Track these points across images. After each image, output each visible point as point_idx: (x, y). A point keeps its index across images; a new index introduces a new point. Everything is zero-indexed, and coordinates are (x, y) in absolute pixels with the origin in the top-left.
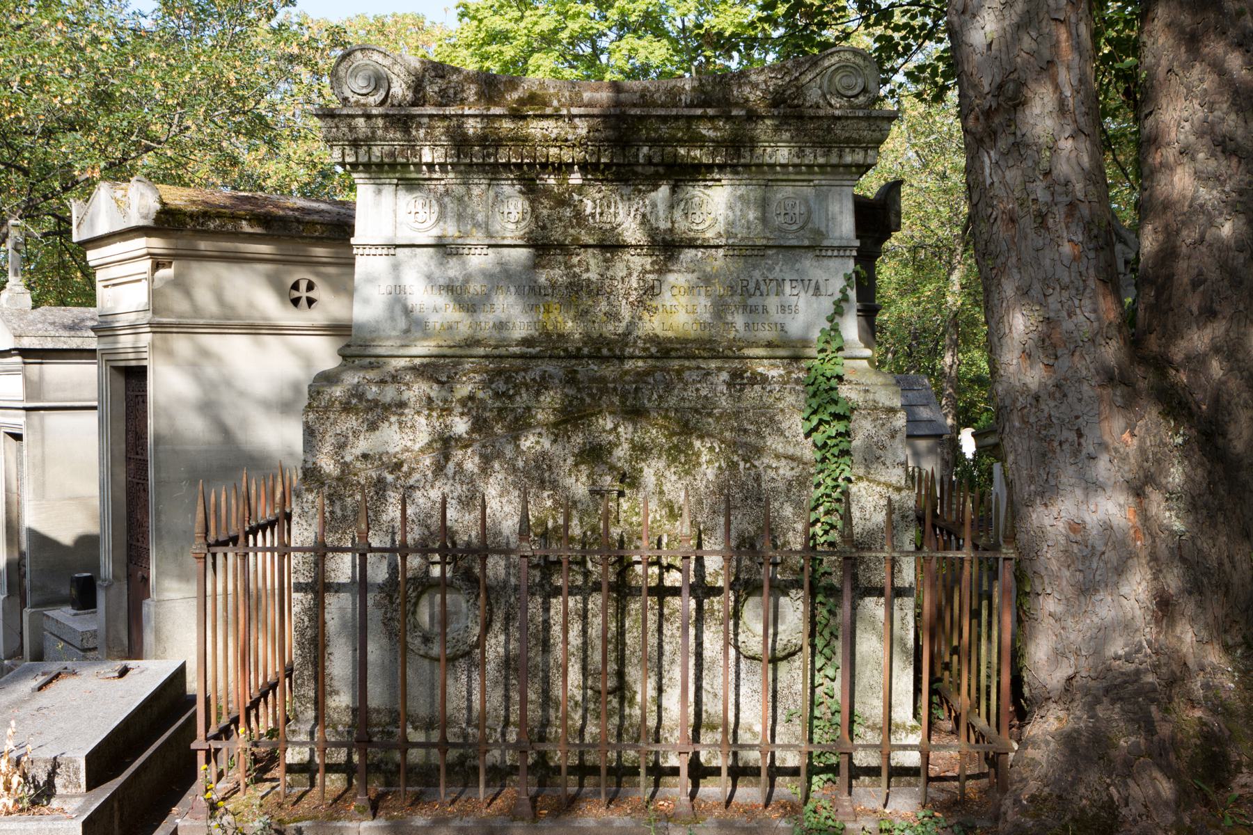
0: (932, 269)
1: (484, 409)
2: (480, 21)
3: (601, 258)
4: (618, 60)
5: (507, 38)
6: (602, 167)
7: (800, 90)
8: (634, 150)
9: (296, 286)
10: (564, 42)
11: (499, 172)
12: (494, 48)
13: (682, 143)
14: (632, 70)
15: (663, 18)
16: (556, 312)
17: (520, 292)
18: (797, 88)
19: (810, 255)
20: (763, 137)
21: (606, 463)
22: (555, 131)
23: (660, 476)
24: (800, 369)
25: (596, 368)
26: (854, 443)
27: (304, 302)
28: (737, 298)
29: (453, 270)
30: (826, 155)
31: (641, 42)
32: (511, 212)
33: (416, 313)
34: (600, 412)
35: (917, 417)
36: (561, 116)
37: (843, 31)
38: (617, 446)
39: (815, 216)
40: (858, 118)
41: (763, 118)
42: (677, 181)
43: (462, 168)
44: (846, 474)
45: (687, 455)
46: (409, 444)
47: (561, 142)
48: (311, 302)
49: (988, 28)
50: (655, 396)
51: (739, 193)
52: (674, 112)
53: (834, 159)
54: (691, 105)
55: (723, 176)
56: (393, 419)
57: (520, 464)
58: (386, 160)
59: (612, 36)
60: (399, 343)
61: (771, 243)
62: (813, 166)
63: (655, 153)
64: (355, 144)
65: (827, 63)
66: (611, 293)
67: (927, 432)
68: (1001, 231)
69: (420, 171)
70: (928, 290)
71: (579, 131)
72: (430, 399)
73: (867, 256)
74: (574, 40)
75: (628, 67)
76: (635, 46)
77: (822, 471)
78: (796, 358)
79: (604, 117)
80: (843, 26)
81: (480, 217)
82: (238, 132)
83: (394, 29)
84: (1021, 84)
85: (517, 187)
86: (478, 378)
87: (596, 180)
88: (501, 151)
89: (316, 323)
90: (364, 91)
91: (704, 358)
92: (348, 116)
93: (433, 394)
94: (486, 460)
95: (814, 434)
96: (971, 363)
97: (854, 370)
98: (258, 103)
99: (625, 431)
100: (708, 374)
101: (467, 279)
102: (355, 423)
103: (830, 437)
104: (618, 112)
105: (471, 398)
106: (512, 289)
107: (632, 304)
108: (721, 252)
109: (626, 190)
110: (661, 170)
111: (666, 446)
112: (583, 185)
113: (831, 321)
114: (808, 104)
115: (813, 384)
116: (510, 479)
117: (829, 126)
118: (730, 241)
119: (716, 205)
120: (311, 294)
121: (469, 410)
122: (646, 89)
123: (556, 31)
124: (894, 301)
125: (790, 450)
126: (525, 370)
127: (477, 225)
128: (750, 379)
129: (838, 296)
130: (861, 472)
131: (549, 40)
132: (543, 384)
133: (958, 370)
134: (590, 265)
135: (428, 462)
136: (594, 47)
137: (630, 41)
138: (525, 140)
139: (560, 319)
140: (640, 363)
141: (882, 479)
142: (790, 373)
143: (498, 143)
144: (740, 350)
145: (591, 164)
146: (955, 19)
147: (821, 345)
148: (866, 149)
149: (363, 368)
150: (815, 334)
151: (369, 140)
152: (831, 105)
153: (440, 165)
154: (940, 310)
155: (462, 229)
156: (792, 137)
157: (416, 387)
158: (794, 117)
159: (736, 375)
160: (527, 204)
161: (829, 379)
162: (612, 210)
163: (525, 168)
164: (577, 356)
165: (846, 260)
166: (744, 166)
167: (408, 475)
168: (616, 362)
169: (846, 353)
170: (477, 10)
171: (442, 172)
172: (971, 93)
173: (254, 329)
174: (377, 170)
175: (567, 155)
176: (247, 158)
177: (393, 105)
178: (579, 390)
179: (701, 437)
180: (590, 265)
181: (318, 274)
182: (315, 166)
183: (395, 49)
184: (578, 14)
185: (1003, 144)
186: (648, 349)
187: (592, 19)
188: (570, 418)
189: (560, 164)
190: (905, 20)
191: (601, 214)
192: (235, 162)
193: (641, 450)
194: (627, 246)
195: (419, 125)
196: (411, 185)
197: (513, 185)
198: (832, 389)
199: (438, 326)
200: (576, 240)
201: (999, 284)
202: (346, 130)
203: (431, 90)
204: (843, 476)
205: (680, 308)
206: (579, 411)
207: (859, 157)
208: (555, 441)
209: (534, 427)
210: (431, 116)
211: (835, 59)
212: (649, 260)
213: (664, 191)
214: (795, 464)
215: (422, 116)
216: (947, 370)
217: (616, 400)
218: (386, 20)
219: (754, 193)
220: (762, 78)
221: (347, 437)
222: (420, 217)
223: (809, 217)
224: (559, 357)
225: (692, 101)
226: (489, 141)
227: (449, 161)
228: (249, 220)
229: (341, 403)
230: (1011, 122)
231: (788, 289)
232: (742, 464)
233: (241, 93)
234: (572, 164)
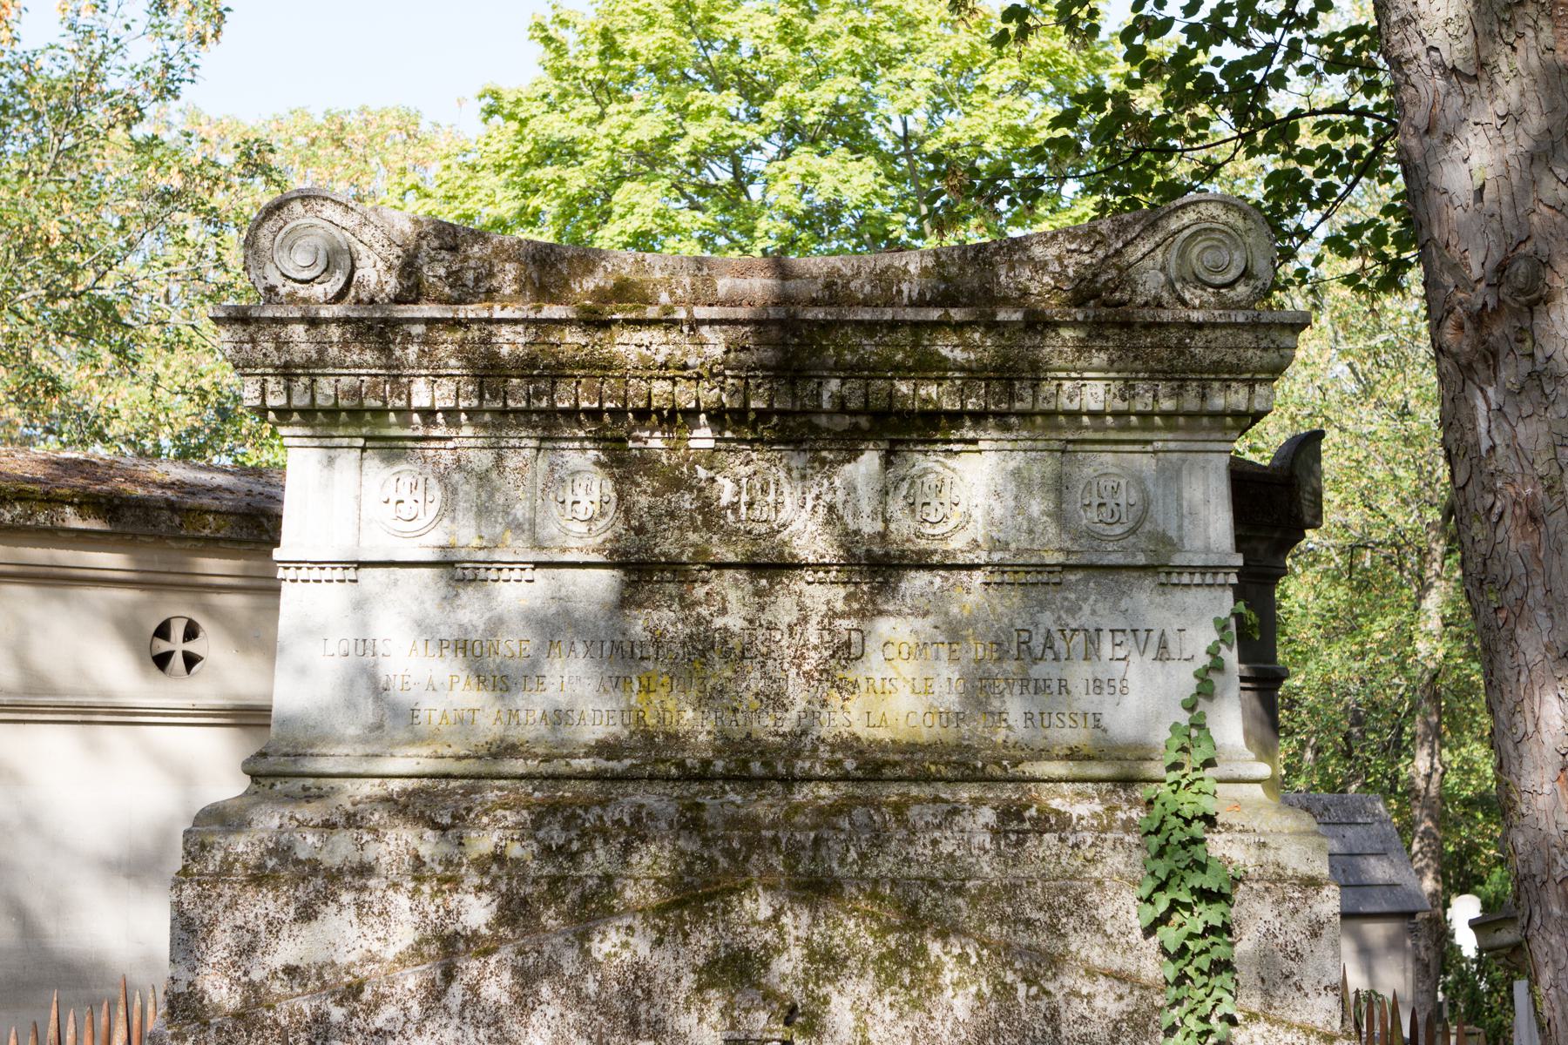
0: (1386, 587)
1: (523, 879)
2: (524, 122)
3: (749, 587)
4: (783, 195)
5: (573, 154)
6: (752, 416)
7: (1125, 277)
8: (812, 385)
9: (163, 631)
10: (682, 161)
11: (558, 427)
12: (547, 173)
13: (902, 371)
14: (808, 214)
15: (868, 116)
16: (663, 691)
17: (593, 645)
18: (1120, 270)
19: (1148, 582)
20: (1056, 362)
21: (758, 986)
22: (664, 350)
23: (863, 1012)
24: (1133, 803)
25: (738, 799)
26: (1239, 948)
27: (177, 662)
28: (1011, 666)
29: (470, 611)
30: (1177, 394)
31: (826, 162)
32: (578, 501)
33: (396, 693)
34: (747, 885)
35: (1365, 878)
36: (675, 322)
37: (1206, 161)
38: (779, 952)
39: (1157, 510)
40: (1236, 325)
41: (1056, 326)
42: (893, 442)
43: (487, 417)
44: (1227, 1007)
45: (914, 971)
46: (376, 947)
47: (675, 370)
48: (191, 660)
49: (1475, 161)
50: (853, 855)
51: (1012, 465)
52: (888, 315)
53: (1191, 402)
54: (920, 303)
55: (982, 435)
56: (346, 897)
57: (591, 987)
58: (344, 403)
59: (771, 150)
60: (360, 749)
61: (1073, 560)
62: (1152, 414)
63: (852, 390)
64: (287, 372)
65: (1174, 224)
66: (767, 656)
67: (1385, 908)
68: (1513, 539)
69: (407, 424)
70: (1380, 629)
71: (708, 350)
72: (418, 862)
73: (1257, 582)
74: (697, 160)
75: (799, 207)
76: (814, 169)
77: (1178, 1002)
78: (1126, 781)
79: (759, 324)
80: (1205, 153)
81: (521, 511)
82: (61, 332)
83: (361, 136)
84: (1543, 264)
85: (592, 454)
86: (511, 818)
87: (741, 441)
88: (561, 386)
89: (201, 703)
90: (306, 275)
91: (948, 781)
92: (275, 320)
93: (425, 851)
94: (527, 978)
95: (1162, 929)
96: (1468, 768)
97: (1238, 805)
98: (101, 276)
99: (797, 923)
100: (955, 811)
101: (496, 625)
102: (271, 906)
103: (1192, 936)
104: (782, 315)
105: (498, 857)
106: (580, 648)
107: (808, 676)
108: (979, 577)
109: (798, 461)
110: (864, 422)
111: (875, 953)
112: (715, 450)
113: (1191, 709)
114: (1140, 300)
115: (1158, 831)
116: (571, 1016)
117: (1180, 340)
118: (996, 557)
119: (973, 489)
120: (193, 647)
121: (494, 881)
122: (834, 272)
123: (666, 141)
124: (1315, 650)
125: (1116, 962)
126: (602, 804)
127: (516, 526)
128: (1035, 821)
129: (1206, 660)
130: (1255, 1004)
131: (651, 157)
132: (637, 831)
133: (1442, 783)
134: (729, 604)
135: (411, 983)
136: (737, 170)
137: (804, 158)
138: (607, 366)
139: (670, 705)
140: (824, 790)
141: (1296, 1019)
142: (1112, 809)
143: (557, 372)
144: (1015, 765)
145: (731, 411)
146: (1413, 142)
147: (1173, 756)
148: (1251, 384)
149: (290, 798)
150: (1161, 735)
151: (314, 366)
152: (1184, 303)
153: (447, 412)
154: (1403, 668)
155: (486, 532)
156: (1111, 362)
157: (391, 835)
158: (1114, 324)
159: (1010, 814)
160: (609, 485)
161: (1188, 823)
162: (771, 498)
163: (607, 418)
164: (703, 775)
165: (1218, 592)
166: (1021, 414)
167: (373, 1007)
168: (778, 787)
169: (1221, 771)
170: (518, 102)
171: (448, 424)
172: (1448, 280)
173: (88, 713)
174: (323, 420)
175: (686, 395)
176: (74, 375)
177: (359, 302)
178: (706, 843)
179: (942, 935)
180: (729, 604)
181: (209, 611)
182: (204, 395)
183: (363, 173)
184: (708, 111)
185: (1510, 373)
186: (839, 763)
187: (733, 118)
188: (692, 897)
189: (673, 412)
190: (1324, 139)
191: (750, 505)
192: (54, 387)
193: (826, 962)
194: (800, 566)
195: (408, 339)
196: (391, 449)
197: (584, 450)
198: (1195, 841)
199: (436, 718)
200: (701, 552)
201: (1512, 638)
202: (270, 346)
203: (434, 273)
204: (1219, 1011)
205: (899, 684)
206: (707, 883)
207: (1237, 398)
208: (659, 943)
209: (620, 915)
210: (430, 322)
211: (1189, 217)
212: (841, 591)
213: (869, 461)
214: (1125, 989)
215: (414, 321)
216: (1421, 784)
217: (777, 861)
218: (347, 119)
219: (1044, 467)
220: (1053, 251)
221: (256, 934)
222: (405, 511)
223: (1145, 511)
224: (668, 778)
225: (921, 294)
227: (463, 404)
228: (80, 506)
229: (245, 866)
230: (1524, 334)
231: (1106, 648)
232: (1022, 989)
233: (71, 258)
234: (695, 412)
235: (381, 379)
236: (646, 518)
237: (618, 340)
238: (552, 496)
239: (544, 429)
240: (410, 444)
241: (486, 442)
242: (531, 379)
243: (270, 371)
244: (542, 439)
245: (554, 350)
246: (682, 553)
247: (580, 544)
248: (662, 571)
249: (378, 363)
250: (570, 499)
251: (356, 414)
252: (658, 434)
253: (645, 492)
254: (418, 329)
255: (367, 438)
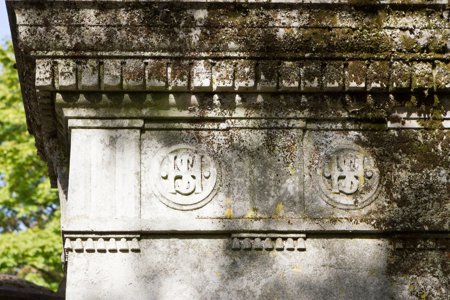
22: (426, 33)
43: (260, 99)
138: (374, 48)
163: (370, 99)
196: (169, 132)
197: (345, 131)
202: (62, 29)
222: (182, 186)
226: (319, 51)
227: (239, 84)
235: (163, 61)
236: (407, 191)
237: (385, 24)
238: (319, 172)
239: (311, 110)
240: (185, 125)
241: (257, 123)
242: (301, 61)
243: (61, 53)
244: (308, 120)
245: (326, 33)
246: (444, 222)
247: (347, 215)
248: (425, 239)
249: (163, 45)
250: (336, 174)
251: (138, 95)
252: (414, 115)
253: (405, 168)
254: (201, 14)
255: (147, 120)
